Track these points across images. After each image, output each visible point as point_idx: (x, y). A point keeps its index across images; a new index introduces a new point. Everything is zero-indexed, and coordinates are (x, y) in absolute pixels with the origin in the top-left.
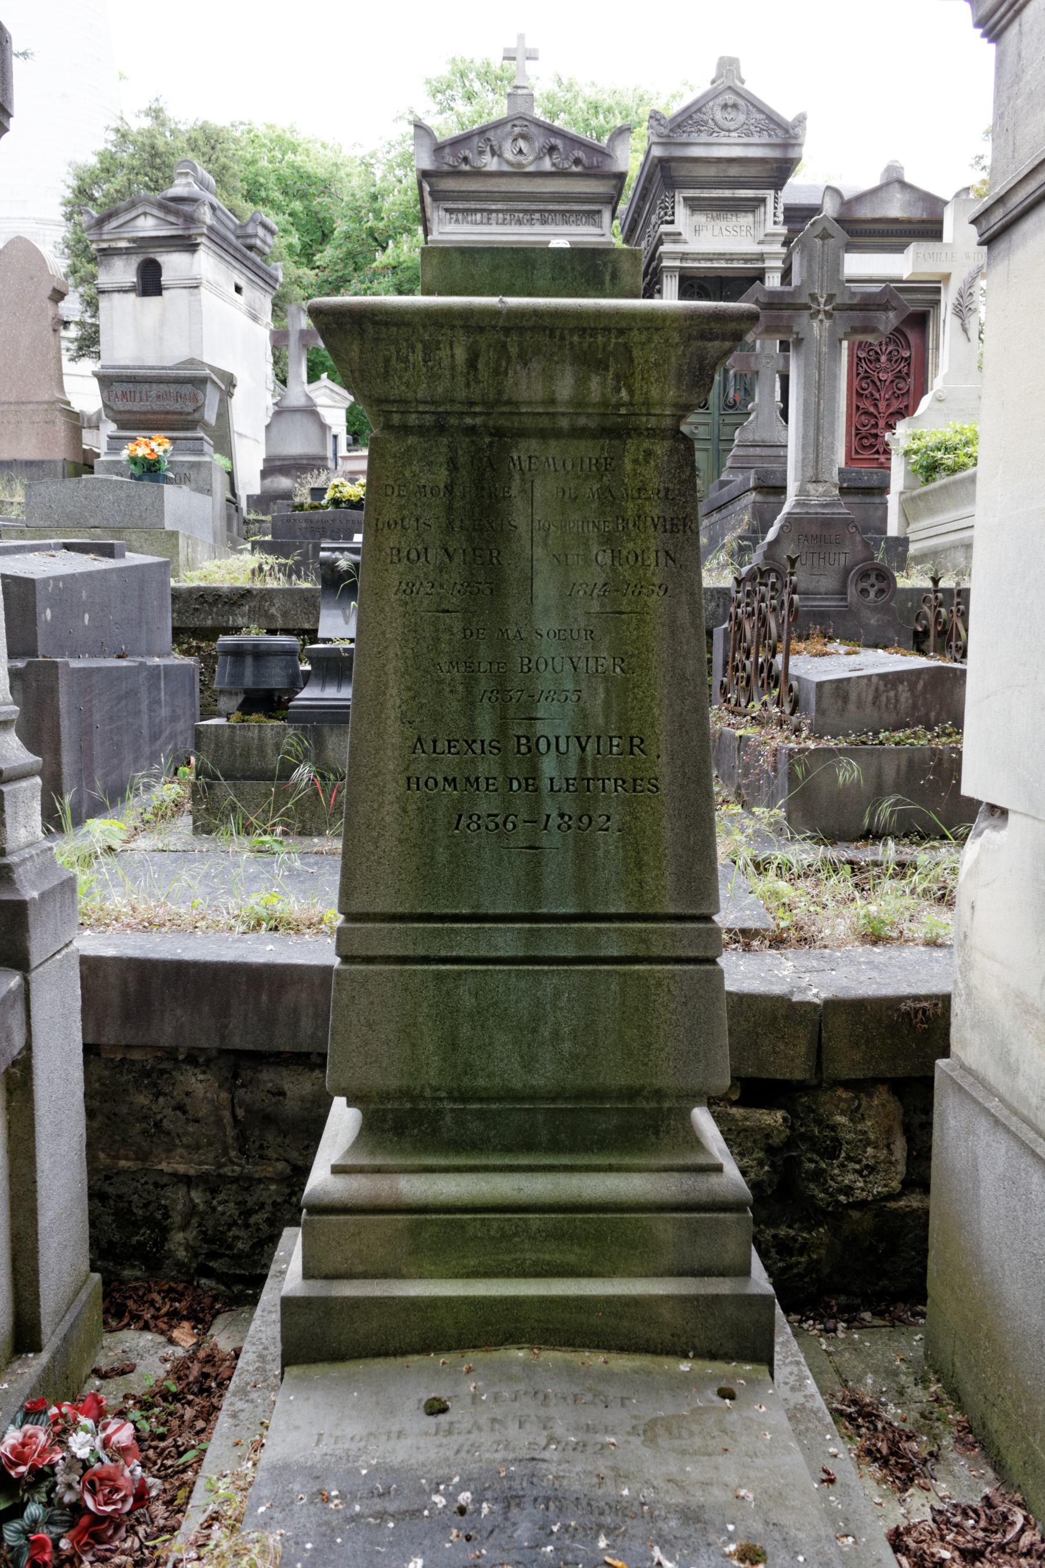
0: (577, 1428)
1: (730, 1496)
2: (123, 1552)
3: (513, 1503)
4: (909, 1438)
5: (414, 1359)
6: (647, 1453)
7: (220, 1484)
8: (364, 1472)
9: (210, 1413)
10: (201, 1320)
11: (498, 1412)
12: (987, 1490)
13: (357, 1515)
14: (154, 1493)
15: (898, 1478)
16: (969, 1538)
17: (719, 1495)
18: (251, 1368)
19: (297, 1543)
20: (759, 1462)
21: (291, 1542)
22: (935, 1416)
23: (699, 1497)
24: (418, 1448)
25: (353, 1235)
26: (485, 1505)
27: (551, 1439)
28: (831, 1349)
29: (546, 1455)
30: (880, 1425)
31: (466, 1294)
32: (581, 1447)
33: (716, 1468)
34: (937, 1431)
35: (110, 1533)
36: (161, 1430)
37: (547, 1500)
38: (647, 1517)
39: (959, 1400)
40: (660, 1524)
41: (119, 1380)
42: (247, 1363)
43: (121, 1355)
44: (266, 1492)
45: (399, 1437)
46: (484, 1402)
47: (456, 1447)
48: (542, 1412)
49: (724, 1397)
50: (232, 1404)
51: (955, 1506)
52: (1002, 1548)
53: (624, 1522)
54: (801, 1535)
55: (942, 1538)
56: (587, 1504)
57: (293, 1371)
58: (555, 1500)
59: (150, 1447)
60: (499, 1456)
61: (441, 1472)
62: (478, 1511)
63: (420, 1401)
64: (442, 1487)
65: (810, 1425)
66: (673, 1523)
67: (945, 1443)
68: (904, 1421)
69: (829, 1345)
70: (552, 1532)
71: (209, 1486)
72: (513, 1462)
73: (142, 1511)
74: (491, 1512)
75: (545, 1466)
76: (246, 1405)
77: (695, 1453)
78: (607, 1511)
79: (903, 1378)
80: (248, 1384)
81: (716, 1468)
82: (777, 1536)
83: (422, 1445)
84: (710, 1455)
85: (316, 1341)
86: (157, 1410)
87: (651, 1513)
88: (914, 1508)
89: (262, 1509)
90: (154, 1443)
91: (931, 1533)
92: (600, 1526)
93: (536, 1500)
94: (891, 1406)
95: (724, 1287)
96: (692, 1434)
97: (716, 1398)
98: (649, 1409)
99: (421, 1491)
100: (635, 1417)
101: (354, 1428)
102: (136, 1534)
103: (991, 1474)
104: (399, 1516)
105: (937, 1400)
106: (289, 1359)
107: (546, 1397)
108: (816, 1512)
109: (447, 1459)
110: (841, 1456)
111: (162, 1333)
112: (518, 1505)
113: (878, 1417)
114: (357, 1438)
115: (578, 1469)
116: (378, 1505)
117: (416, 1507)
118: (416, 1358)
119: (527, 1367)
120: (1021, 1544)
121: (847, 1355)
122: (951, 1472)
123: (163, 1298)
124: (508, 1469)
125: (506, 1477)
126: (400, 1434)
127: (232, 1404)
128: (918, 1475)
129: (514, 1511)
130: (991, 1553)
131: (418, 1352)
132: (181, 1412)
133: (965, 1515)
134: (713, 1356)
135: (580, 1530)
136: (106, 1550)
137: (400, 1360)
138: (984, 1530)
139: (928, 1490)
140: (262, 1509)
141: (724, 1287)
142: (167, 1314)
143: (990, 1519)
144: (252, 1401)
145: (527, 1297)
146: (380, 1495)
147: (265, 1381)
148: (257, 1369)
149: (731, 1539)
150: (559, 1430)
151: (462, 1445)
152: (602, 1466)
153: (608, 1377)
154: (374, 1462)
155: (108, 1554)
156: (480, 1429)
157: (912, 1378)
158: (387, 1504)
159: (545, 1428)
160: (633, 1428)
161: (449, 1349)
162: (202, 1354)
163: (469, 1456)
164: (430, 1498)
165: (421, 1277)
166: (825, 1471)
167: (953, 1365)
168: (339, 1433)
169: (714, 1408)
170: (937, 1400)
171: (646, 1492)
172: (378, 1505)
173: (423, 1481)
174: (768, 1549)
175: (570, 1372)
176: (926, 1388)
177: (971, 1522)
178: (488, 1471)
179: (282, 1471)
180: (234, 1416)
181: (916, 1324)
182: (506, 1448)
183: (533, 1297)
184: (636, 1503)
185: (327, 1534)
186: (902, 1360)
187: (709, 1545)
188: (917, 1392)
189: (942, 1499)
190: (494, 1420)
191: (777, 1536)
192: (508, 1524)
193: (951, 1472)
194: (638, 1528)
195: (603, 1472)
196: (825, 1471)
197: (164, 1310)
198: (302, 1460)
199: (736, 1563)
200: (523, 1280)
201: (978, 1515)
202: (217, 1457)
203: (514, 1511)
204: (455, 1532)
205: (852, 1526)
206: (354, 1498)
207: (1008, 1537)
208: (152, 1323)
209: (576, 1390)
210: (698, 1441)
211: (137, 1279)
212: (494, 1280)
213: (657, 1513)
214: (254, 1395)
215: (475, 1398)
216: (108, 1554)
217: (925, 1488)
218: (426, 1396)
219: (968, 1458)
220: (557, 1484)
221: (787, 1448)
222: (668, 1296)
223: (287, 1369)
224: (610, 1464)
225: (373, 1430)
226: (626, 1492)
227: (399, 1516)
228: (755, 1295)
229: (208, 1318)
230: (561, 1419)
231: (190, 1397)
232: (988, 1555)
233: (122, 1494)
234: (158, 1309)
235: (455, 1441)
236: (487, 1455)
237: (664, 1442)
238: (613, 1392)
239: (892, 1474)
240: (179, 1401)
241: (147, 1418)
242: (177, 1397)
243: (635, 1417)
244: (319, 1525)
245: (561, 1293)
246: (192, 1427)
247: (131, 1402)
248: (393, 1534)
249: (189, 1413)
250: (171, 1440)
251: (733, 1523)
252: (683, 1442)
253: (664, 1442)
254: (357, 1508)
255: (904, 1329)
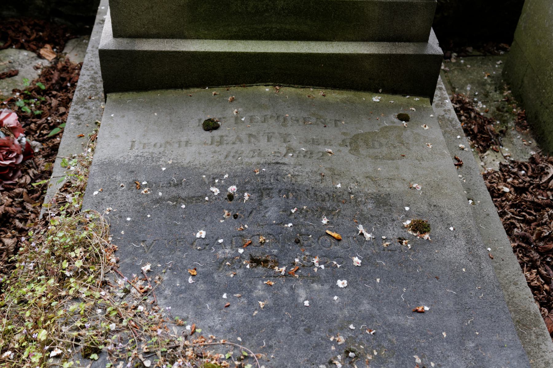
0: (306, 141)
1: (407, 187)
2: (21, 186)
3: (264, 193)
4: (490, 123)
5: (195, 91)
6: (352, 158)
7: (71, 163)
8: (164, 169)
9: (66, 102)
10: (59, 45)
11: (253, 130)
12: (533, 153)
13: (160, 198)
14: (37, 150)
15: (481, 145)
16: (520, 180)
17: (399, 187)
18: (87, 86)
19: (120, 217)
20: (425, 164)
21: (117, 216)
22: (505, 109)
23: (386, 188)
24: (200, 154)
25: (147, 8)
26: (246, 194)
27: (289, 149)
28: (447, 69)
29: (286, 160)
30: (473, 115)
31: (230, 51)
32: (309, 154)
33: (397, 168)
34: (506, 118)
35: (11, 175)
36: (38, 112)
37: (287, 191)
38: (353, 203)
39: (522, 101)
40: (362, 207)
41: (9, 80)
42: (84, 83)
43: (8, 64)
44: (98, 181)
45: (186, 145)
46: (243, 122)
47: (225, 154)
48: (283, 130)
49: (402, 120)
50: (75, 110)
51: (513, 162)
52: (538, 186)
53: (339, 206)
54: (452, 213)
55: (505, 181)
56: (313, 193)
57: (112, 96)
58: (293, 192)
59: (32, 122)
60: (255, 160)
61: (215, 170)
62: (242, 198)
63: (200, 120)
64: (217, 181)
65: (447, 129)
66: (370, 206)
67: (509, 125)
68: (487, 112)
69: (445, 67)
70: (291, 213)
71: (63, 165)
72: (264, 165)
73: (30, 161)
74: (250, 199)
75: (285, 168)
76: (85, 111)
77: (383, 158)
78: (327, 199)
79: (488, 87)
80: (85, 96)
81: (397, 168)
82: (436, 213)
83: (202, 151)
84: (393, 159)
85: (125, 76)
86: (33, 101)
87: (356, 199)
88: (489, 162)
89: (96, 193)
90: (34, 120)
91: (499, 178)
92: (323, 209)
93: (280, 191)
94: (480, 103)
95: (409, 49)
96: (381, 145)
97: (396, 120)
98: (352, 127)
99: (203, 183)
100: (344, 134)
101: (155, 138)
102: (28, 174)
103: (534, 144)
104: (188, 200)
105: (508, 100)
106: (108, 90)
107: (285, 119)
108: (461, 197)
109: (219, 162)
110: (466, 149)
111: (33, 51)
112: (268, 195)
113: (472, 110)
114: (158, 145)
115: (308, 170)
116: (174, 192)
117: (199, 194)
118: (196, 90)
119: (271, 97)
120: (550, 184)
121: (456, 72)
122: (511, 142)
123: (31, 30)
124: (260, 170)
125: (258, 175)
126: (187, 143)
127: (75, 110)
128: (493, 143)
129: (266, 199)
130: (532, 189)
131: (197, 87)
132: (49, 101)
133: (520, 169)
134: (394, 92)
135: (310, 212)
136: (10, 184)
137: (185, 91)
138: (530, 177)
139: (498, 152)
140: (96, 193)
141: (409, 49)
142: (35, 39)
143: (533, 170)
144: (89, 108)
145: (273, 53)
146: (176, 185)
147: (96, 95)
148: (91, 87)
149: (408, 216)
150: (294, 143)
151: (230, 152)
152: (323, 167)
153: (326, 106)
154: (170, 162)
155: (12, 187)
156: (241, 141)
157: (493, 87)
158: (180, 192)
159: (285, 141)
160: (343, 141)
161: (218, 85)
162: (59, 66)
163: (234, 160)
164: (209, 188)
165: (198, 38)
166: (456, 159)
167: (523, 81)
168: (146, 141)
169: (395, 127)
170: (508, 100)
171: (352, 185)
172: (174, 192)
173: (204, 176)
174: (431, 223)
175: (301, 102)
176: (501, 93)
177: (523, 172)
178: (247, 170)
179: (108, 166)
180: (77, 118)
181: (499, 54)
182: (259, 155)
183: (277, 53)
184: (346, 193)
185: (141, 211)
186: (488, 76)
187: (393, 220)
188: (496, 95)
189: (505, 157)
190: (250, 135)
191: (436, 213)
192: (261, 208)
193: (511, 142)
194: (348, 210)
195: (324, 172)
196: (456, 159)
197: (32, 38)
198: (122, 159)
199: (410, 232)
200: (270, 42)
201: (527, 168)
202: (68, 145)
203: (266, 199)
204: (226, 212)
205: (472, 193)
206: (158, 187)
207: (543, 181)
208: (26, 45)
209: (305, 115)
210: (385, 150)
211: (13, 17)
212: (250, 42)
213: (359, 199)
214: (90, 104)
215: (237, 119)
216: (12, 187)
217: (496, 151)
218: (204, 118)
219: (522, 134)
220: (294, 180)
221: (442, 154)
222: (370, 55)
223: (108, 95)
224: (328, 166)
225: (169, 140)
226: (339, 186)
227: (188, 200)
228: (430, 55)
229: (62, 42)
230: (295, 135)
231: (54, 93)
232: (530, 190)
233: (15, 154)
234: (29, 36)
235: (225, 149)
236: (247, 160)
237: (363, 151)
238: (329, 116)
239: (478, 143)
240: (48, 95)
241: (29, 104)
242: (45, 93)
243: (344, 134)
244: (135, 205)
245: (296, 51)
246: (58, 110)
247: (18, 94)
248: (185, 212)
249: (54, 102)
250: (44, 119)
251: (408, 206)
252: (376, 151)
253: (363, 151)
254: (160, 194)
255: (491, 58)
